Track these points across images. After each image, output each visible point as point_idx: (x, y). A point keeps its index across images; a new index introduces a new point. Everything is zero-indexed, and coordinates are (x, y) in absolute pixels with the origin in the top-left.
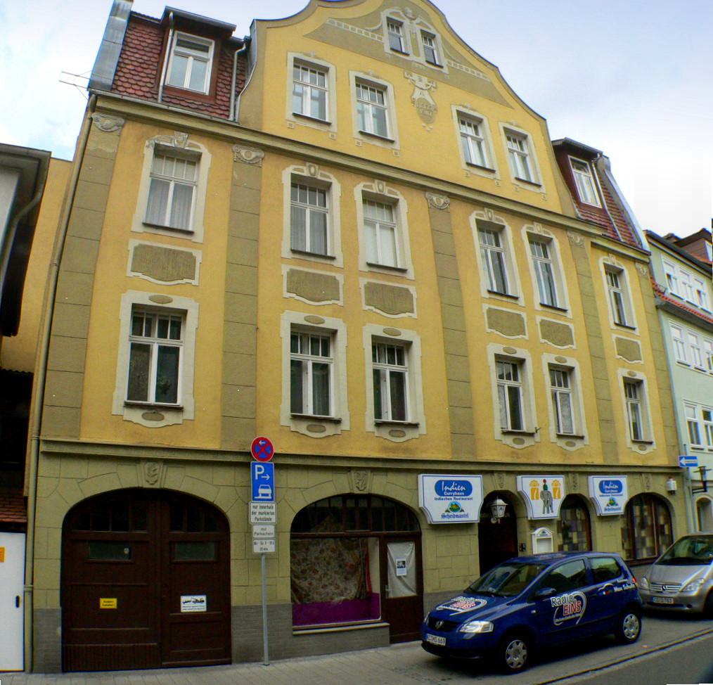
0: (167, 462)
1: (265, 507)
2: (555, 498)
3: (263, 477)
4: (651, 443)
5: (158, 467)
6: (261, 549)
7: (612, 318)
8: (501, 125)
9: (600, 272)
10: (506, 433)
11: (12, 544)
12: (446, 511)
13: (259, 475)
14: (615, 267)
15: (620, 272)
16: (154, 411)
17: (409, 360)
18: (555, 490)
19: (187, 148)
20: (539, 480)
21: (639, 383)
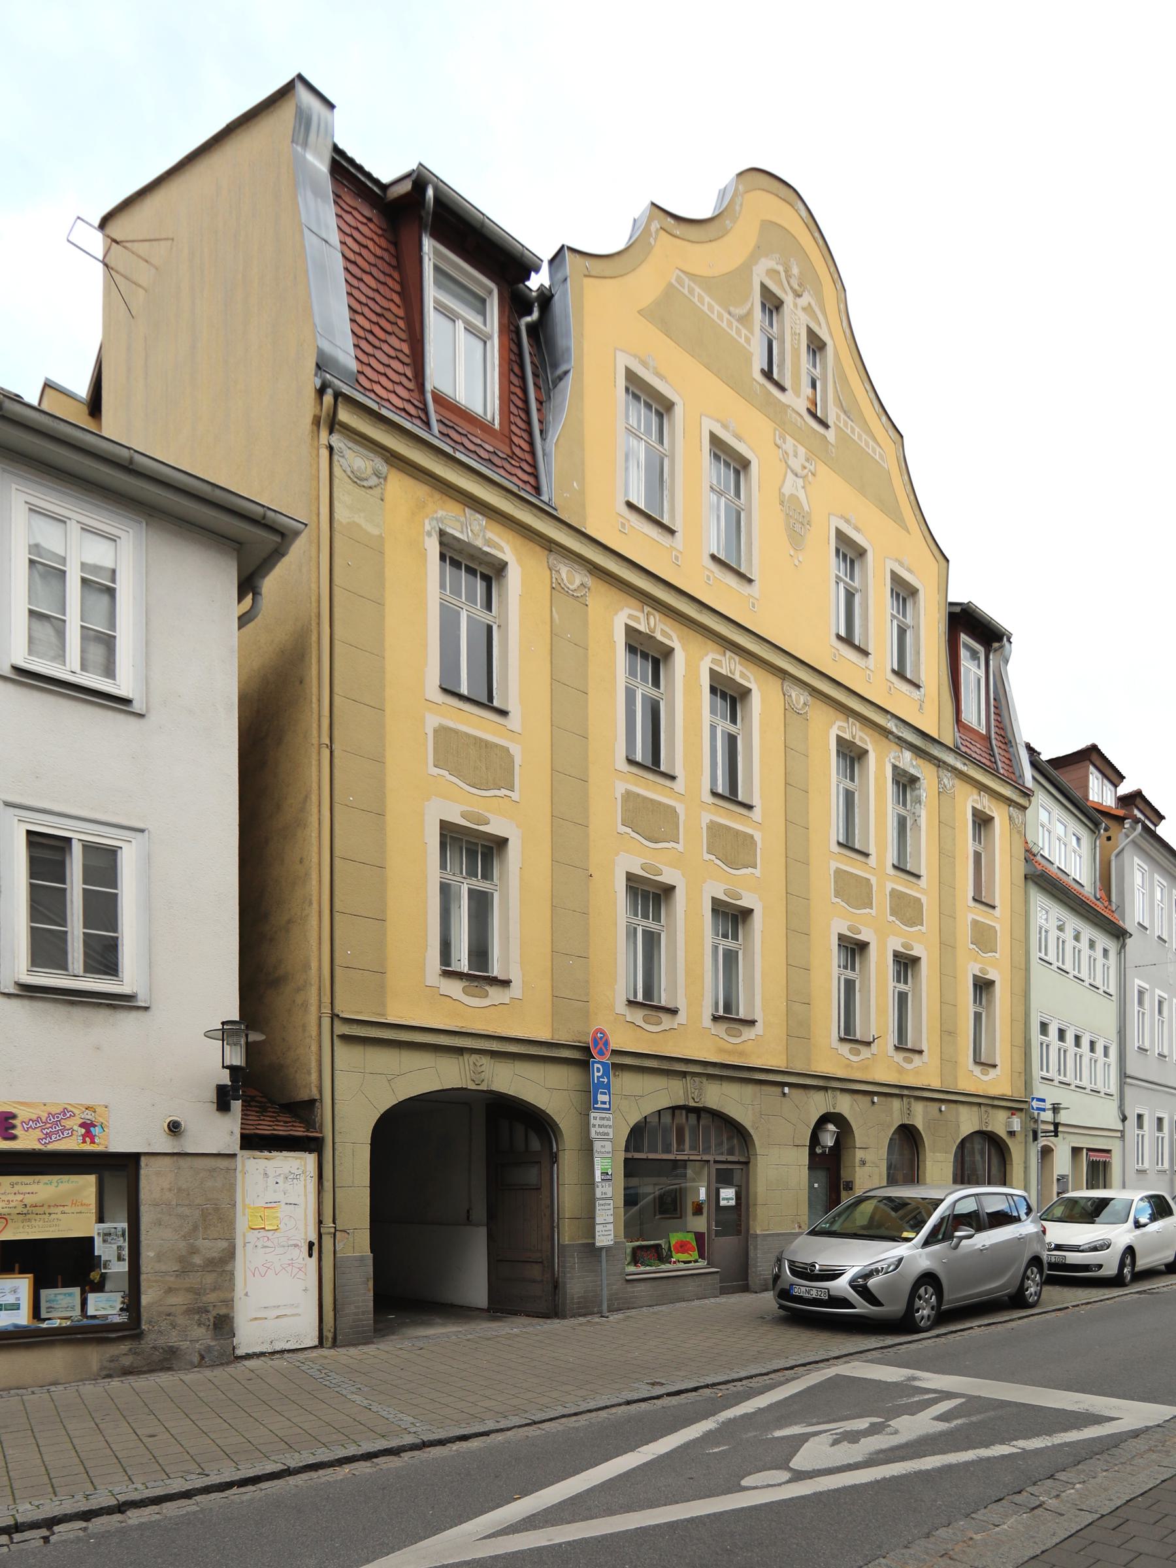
0: (494, 1054)
4: (995, 1066)
5: (485, 1061)
7: (836, 832)
8: (623, 361)
9: (613, 643)
10: (716, 1019)
14: (985, 813)
15: (863, 753)
16: (476, 984)
17: (667, 915)
21: (863, 946)
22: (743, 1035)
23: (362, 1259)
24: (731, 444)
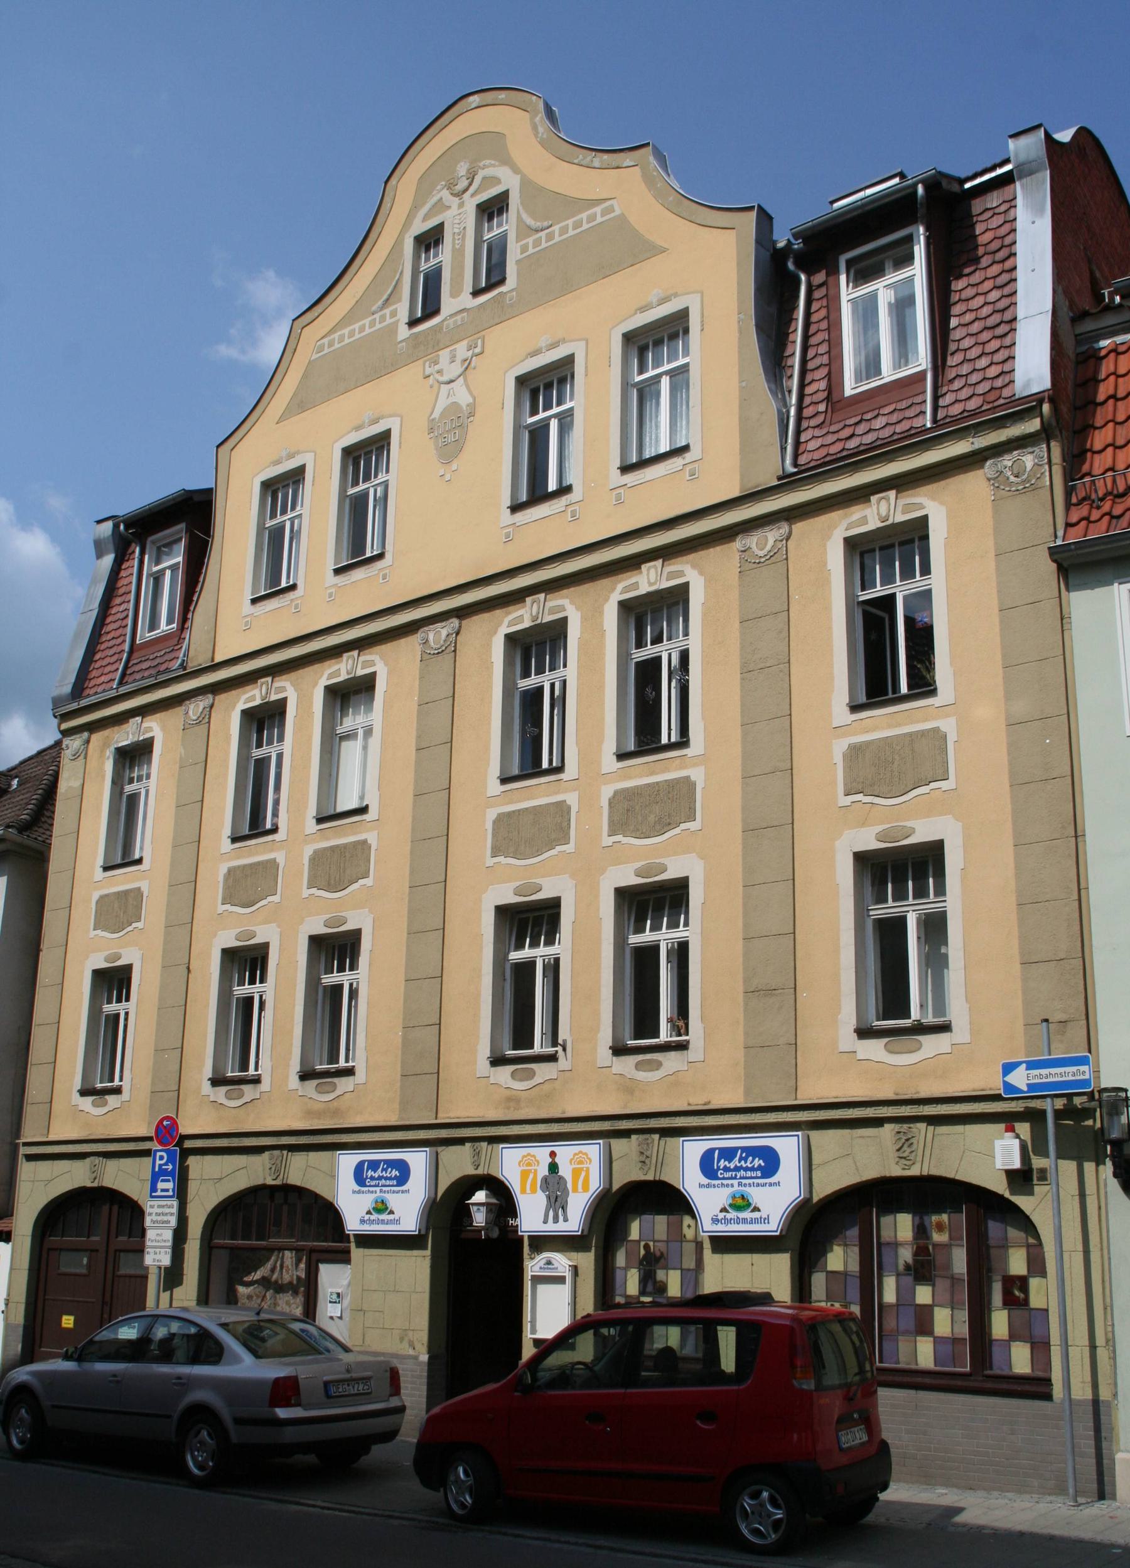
1: (163, 1206)
2: (575, 1190)
3: (164, 1167)
5: (97, 1160)
6: (154, 1260)
11: (4, 1236)
12: (721, 1211)
13: (160, 1165)
18: (576, 1173)
19: (141, 738)
20: (541, 1153)
22: (338, 1088)
23: (19, 1325)
24: (349, 444)
